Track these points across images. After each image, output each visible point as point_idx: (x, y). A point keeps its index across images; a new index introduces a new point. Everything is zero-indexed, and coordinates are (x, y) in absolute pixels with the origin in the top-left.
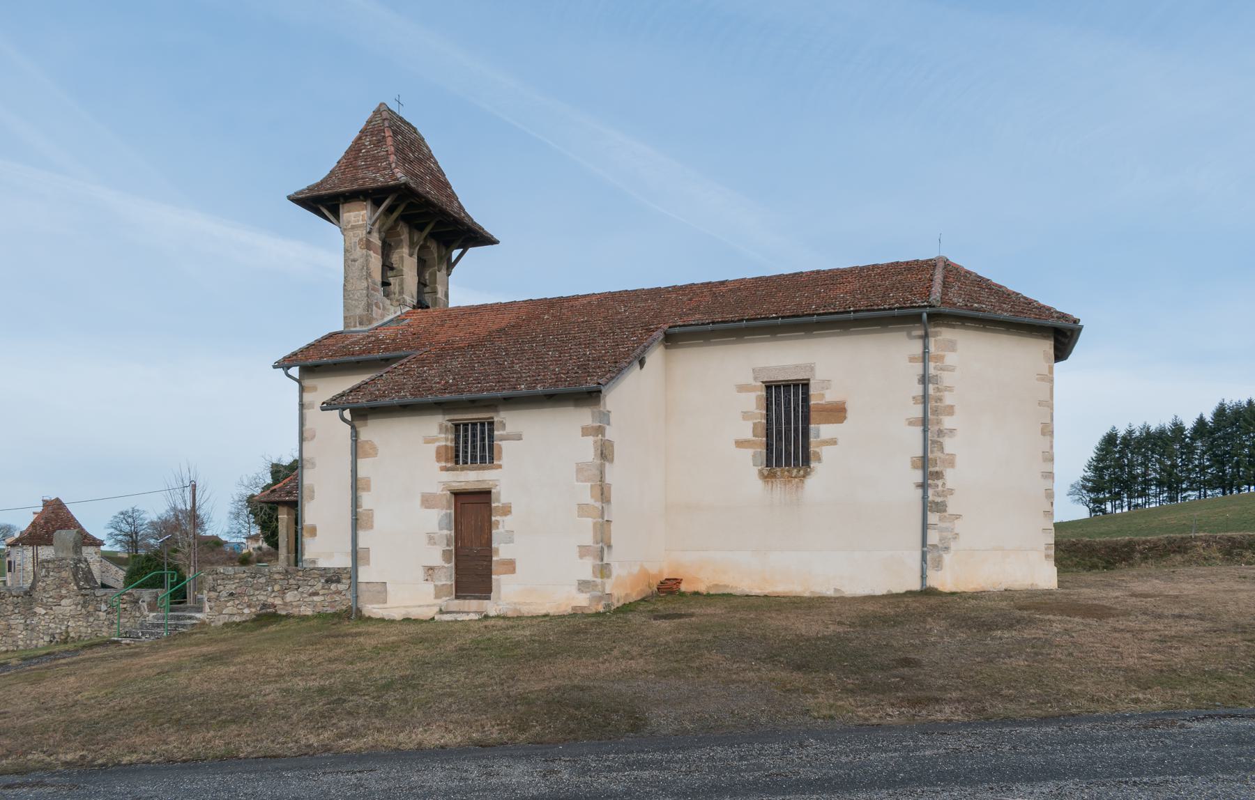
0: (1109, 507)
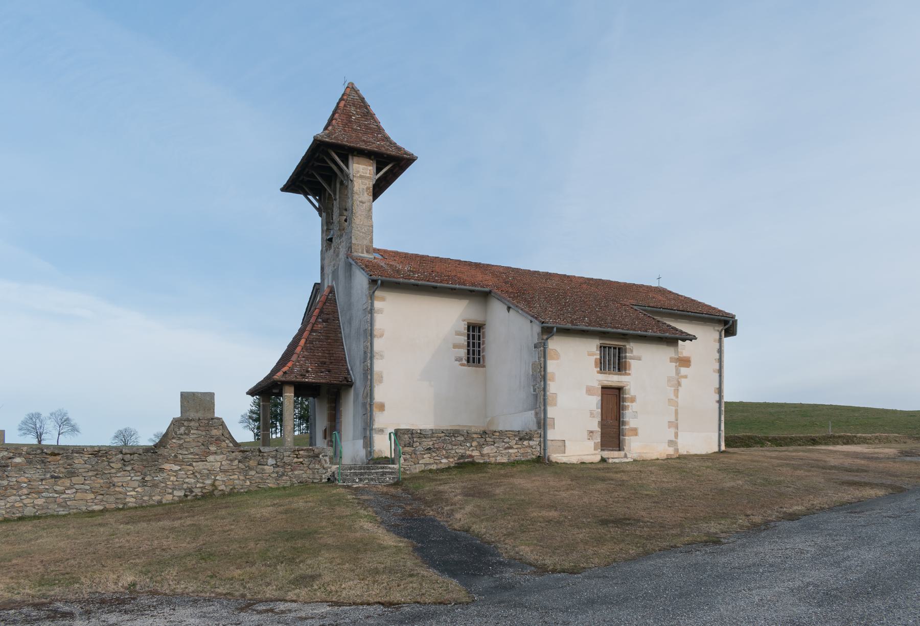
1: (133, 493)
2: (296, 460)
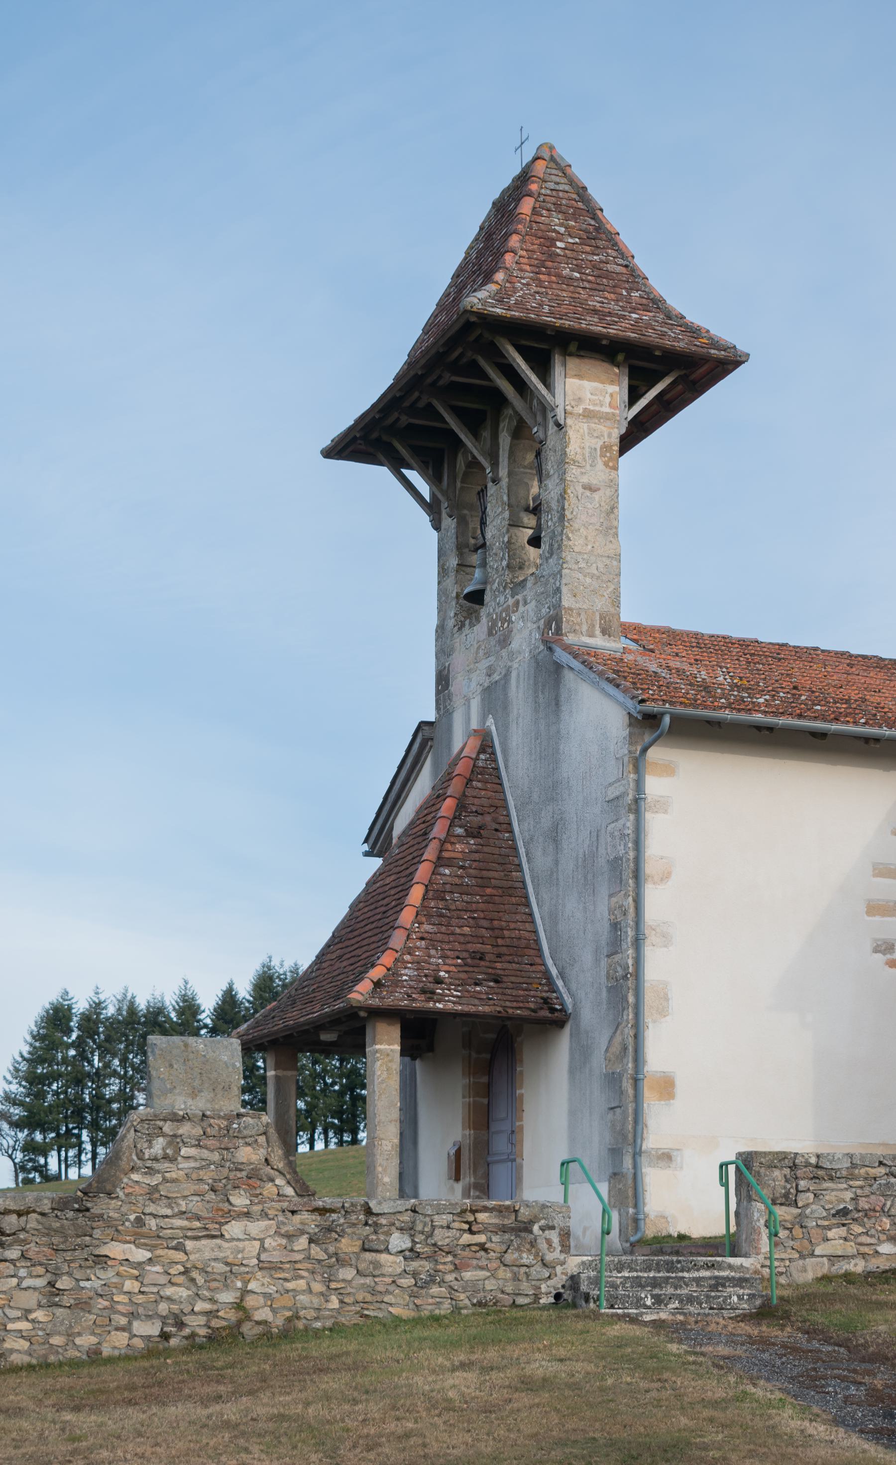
0: (53, 1163)
1: (23, 1325)
2: (466, 1238)
